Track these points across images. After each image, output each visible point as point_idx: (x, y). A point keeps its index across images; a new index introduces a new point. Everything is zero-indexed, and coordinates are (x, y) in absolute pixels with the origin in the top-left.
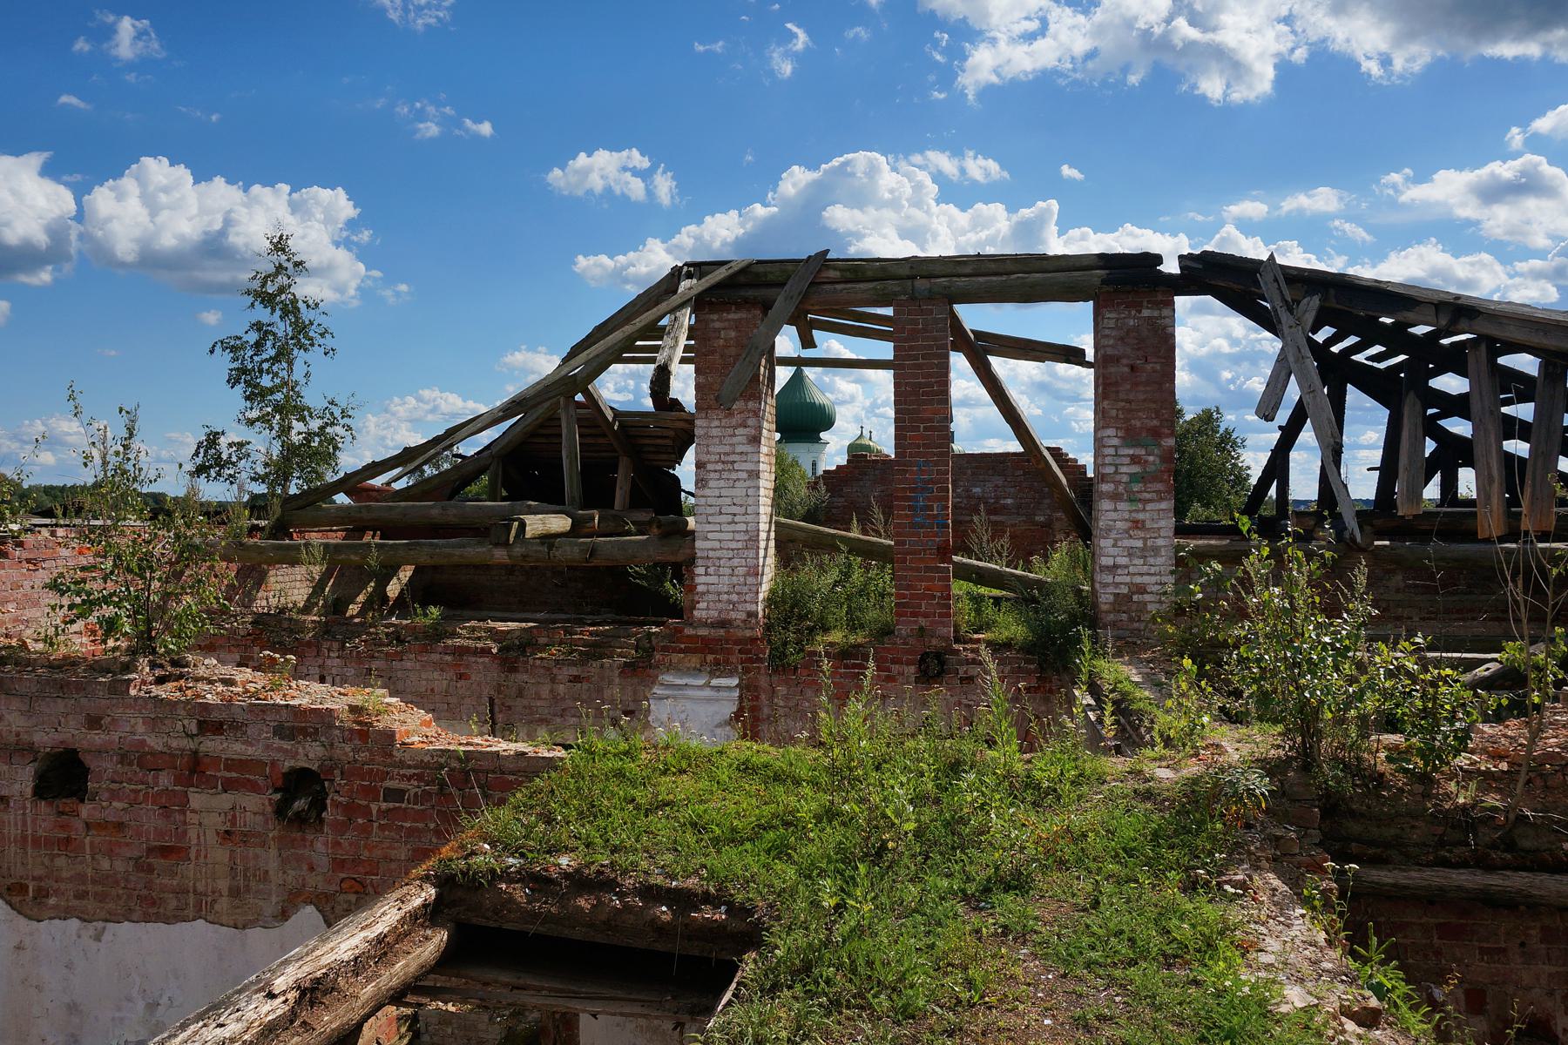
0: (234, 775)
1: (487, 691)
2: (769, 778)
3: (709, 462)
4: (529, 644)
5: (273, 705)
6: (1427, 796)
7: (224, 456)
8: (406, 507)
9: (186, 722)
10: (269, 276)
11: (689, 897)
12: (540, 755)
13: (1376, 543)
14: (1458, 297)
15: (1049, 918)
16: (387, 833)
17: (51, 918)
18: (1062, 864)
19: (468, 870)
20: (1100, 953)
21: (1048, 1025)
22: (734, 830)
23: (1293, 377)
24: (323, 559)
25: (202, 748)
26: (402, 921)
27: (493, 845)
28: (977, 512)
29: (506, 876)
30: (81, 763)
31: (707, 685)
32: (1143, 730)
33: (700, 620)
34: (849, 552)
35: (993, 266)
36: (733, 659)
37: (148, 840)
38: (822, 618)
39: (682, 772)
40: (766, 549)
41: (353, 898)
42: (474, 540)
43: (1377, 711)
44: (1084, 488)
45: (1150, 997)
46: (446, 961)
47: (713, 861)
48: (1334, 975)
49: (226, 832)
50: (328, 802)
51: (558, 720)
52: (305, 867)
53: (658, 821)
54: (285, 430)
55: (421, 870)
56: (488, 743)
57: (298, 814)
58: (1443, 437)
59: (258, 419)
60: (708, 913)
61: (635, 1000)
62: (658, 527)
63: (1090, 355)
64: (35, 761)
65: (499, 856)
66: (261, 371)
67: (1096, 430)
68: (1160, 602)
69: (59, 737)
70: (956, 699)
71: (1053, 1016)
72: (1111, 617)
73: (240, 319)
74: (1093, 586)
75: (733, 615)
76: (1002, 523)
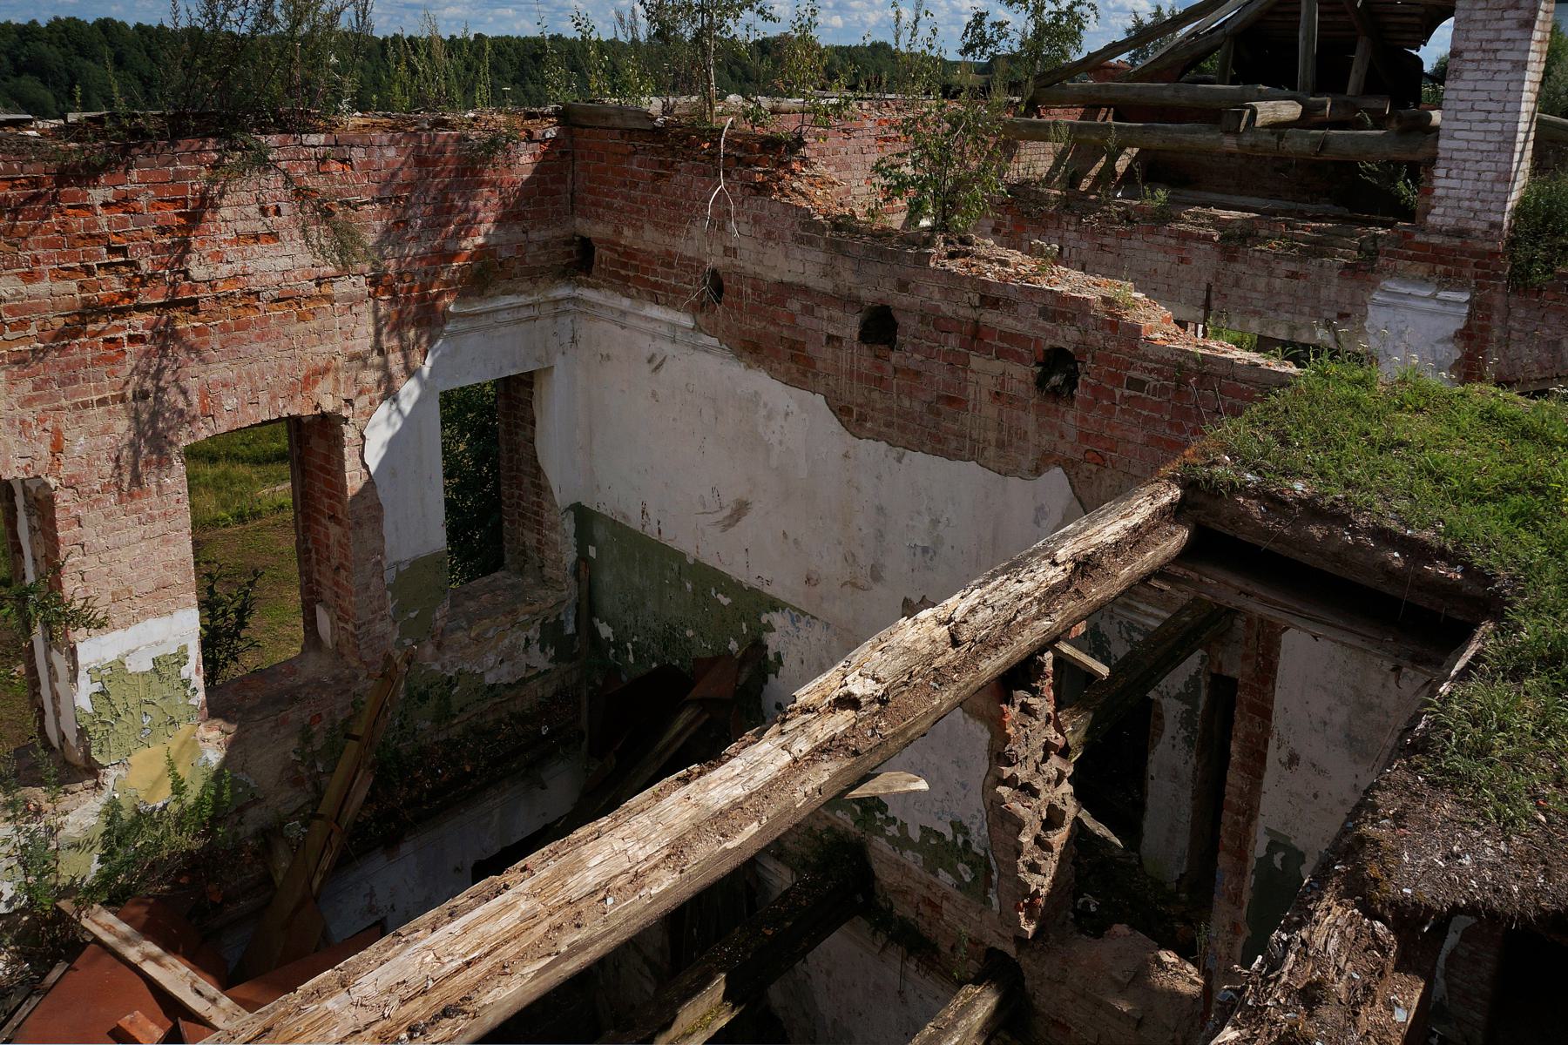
0: (1005, 345)
1: (1206, 278)
2: (1517, 433)
3: (1467, 50)
4: (1250, 235)
7: (987, 36)
9: (971, 295)
11: (1424, 549)
24: (1069, 138)
25: (982, 319)
26: (1153, 515)
27: (1233, 459)
29: (1243, 490)
30: (892, 318)
31: (1433, 297)
33: (1433, 227)
36: (1467, 273)
39: (1419, 410)
40: (1522, 152)
41: (1094, 468)
46: (1187, 555)
47: (1450, 514)
50: (1080, 381)
51: (1271, 314)
52: (1057, 434)
55: (1166, 470)
57: (1054, 388)
62: (1399, 122)
69: (877, 295)
75: (1473, 224)
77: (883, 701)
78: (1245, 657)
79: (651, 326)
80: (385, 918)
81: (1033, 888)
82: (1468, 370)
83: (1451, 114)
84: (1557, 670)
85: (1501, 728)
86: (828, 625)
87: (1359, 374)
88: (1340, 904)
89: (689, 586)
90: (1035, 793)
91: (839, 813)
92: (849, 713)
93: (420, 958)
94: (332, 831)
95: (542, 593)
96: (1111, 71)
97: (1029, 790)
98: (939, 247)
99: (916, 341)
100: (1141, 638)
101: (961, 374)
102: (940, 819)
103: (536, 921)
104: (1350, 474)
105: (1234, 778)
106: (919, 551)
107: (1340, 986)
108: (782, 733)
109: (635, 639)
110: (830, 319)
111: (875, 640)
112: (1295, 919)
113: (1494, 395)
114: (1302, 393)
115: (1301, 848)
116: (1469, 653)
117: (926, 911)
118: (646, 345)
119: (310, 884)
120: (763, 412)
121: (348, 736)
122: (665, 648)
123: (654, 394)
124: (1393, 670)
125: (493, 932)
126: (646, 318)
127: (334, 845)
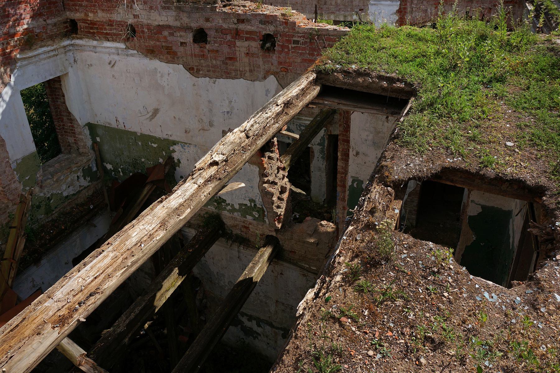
0: (248, 36)
2: (417, 39)
5: (259, 14)
9: (233, 19)
12: (341, 30)
15: (511, 92)
16: (294, 54)
17: (201, 77)
18: (517, 74)
19: (325, 69)
20: (528, 105)
21: (508, 127)
25: (239, 28)
26: (308, 84)
27: (332, 61)
29: (336, 71)
30: (205, 32)
32: (552, 22)
41: (284, 73)
45: (543, 120)
49: (247, 53)
50: (276, 44)
51: (338, 12)
53: (382, 54)
55: (310, 69)
56: (324, 26)
57: (268, 48)
60: (398, 85)
64: (192, 32)
65: (334, 65)
69: (198, 25)
70: (479, 5)
71: (510, 124)
77: (226, 161)
78: (340, 125)
79: (107, 50)
80: (41, 287)
81: (279, 213)
82: (401, 22)
84: (432, 107)
85: (418, 127)
86: (196, 146)
87: (369, 28)
88: (378, 185)
89: (140, 143)
90: (276, 184)
91: (209, 207)
92: (215, 167)
93: (77, 281)
94: (12, 263)
95: (80, 158)
97: (274, 183)
99: (215, 39)
100: (304, 128)
101: (233, 49)
102: (245, 200)
103: (117, 258)
104: (368, 60)
105: (340, 163)
106: (226, 113)
107: (380, 207)
108: (193, 179)
109: (122, 167)
110: (181, 36)
111: (220, 142)
112: (365, 193)
113: (410, 28)
114: (351, 36)
115: (362, 179)
117: (244, 230)
118: (107, 58)
119: (7, 283)
120: (159, 75)
121: (11, 227)
122: (134, 167)
123: (113, 76)
124: (386, 118)
125: (102, 265)
126: (105, 47)
127: (14, 267)
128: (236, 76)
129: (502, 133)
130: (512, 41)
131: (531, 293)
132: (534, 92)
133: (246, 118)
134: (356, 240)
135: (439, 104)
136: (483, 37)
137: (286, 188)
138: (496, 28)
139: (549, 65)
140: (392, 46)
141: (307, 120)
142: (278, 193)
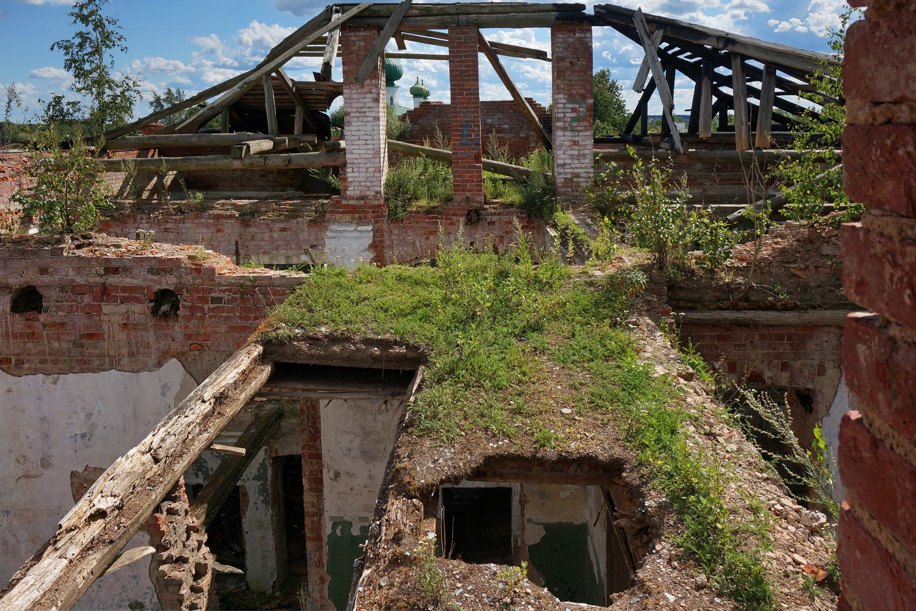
0: (127, 294)
1: (234, 238)
4: (256, 212)
6: (712, 279)
8: (176, 137)
9: (97, 268)
10: (84, 5)
13: (690, 150)
14: (727, 34)
15: (553, 342)
18: (556, 318)
22: (403, 310)
23: (656, 90)
25: (108, 282)
26: (251, 363)
28: (491, 132)
29: (296, 338)
30: (38, 293)
31: (356, 230)
32: (583, 249)
33: (350, 196)
34: (426, 157)
35: (499, 9)
36: (369, 216)
37: (80, 331)
38: (415, 193)
41: (197, 353)
42: (220, 156)
43: (691, 242)
44: (547, 118)
46: (271, 379)
48: (675, 360)
50: (180, 306)
51: (275, 252)
52: (170, 340)
53: (363, 307)
54: (100, 94)
55: (252, 338)
58: (722, 97)
59: (84, 88)
60: (397, 350)
61: (363, 392)
62: (326, 147)
63: (549, 56)
66: (84, 60)
67: (553, 94)
68: (587, 182)
70: (486, 233)
72: (563, 190)
73: (70, 30)
74: (553, 173)
75: (368, 193)
76: (503, 138)
77: (119, 508)
82: (380, 260)
83: (350, 142)
90: (184, 560)
92: (100, 522)
96: (153, 128)
97: (182, 560)
98: (68, 243)
99: (58, 304)
101: (97, 318)
105: (308, 498)
106: (79, 438)
108: (56, 549)
111: (105, 474)
116: (418, 381)
128: (100, 367)
129: (553, 398)
130: (541, 276)
131: (638, 602)
132: (582, 339)
133: (150, 427)
134: (380, 587)
135: (462, 370)
136: (503, 275)
137: (206, 565)
138: (517, 261)
139: (592, 303)
140: (378, 295)
141: (230, 437)
142: (191, 579)
